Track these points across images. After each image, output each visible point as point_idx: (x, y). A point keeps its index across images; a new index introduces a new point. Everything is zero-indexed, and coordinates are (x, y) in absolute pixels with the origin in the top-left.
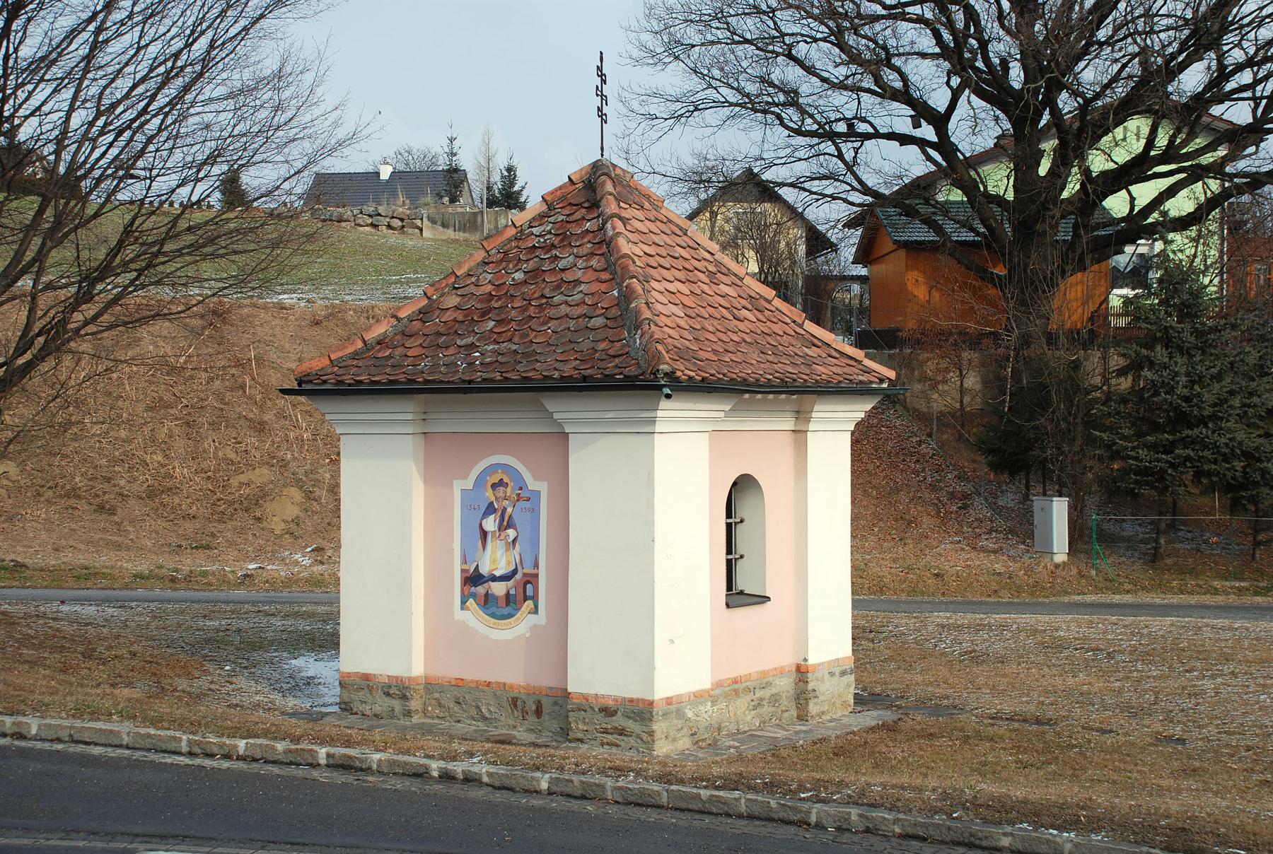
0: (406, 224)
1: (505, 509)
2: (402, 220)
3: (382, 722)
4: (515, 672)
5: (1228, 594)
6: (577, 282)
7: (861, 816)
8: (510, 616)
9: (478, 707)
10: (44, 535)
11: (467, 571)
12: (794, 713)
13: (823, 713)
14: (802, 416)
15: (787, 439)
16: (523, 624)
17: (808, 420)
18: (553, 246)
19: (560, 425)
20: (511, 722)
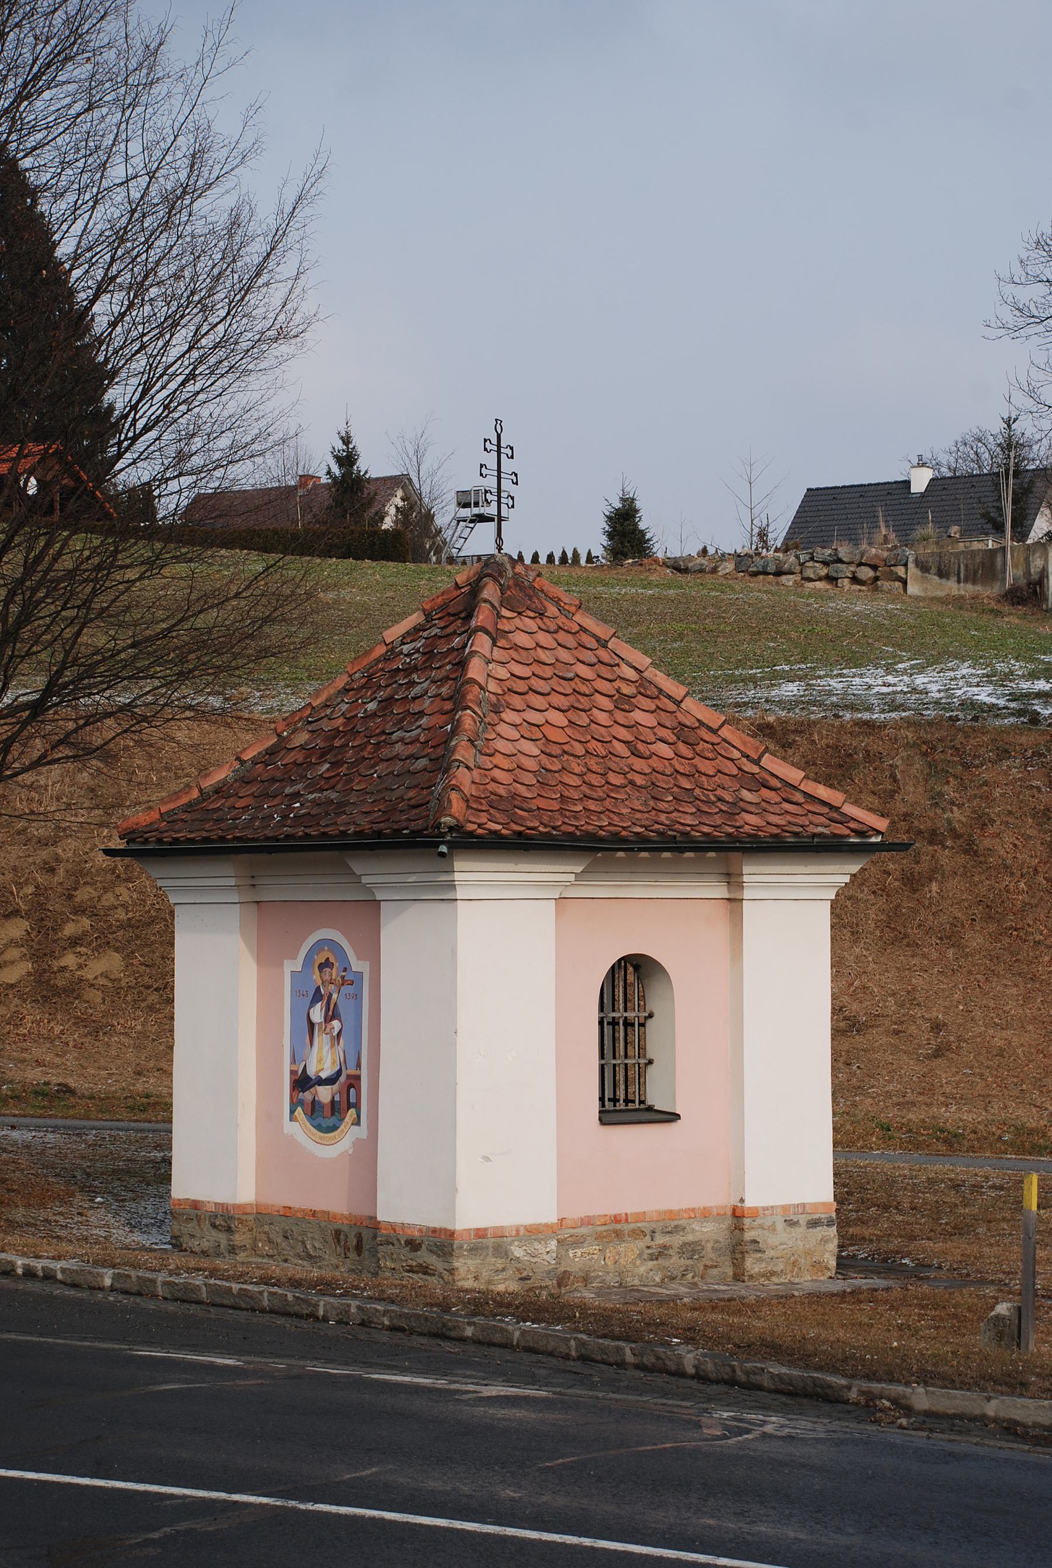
0: (881, 574)
1: (330, 995)
2: (874, 568)
4: (334, 1200)
6: (421, 714)
7: (359, 1307)
8: (334, 1128)
9: (303, 1242)
10: (130, 1055)
12: (730, 1271)
13: (773, 1273)
14: (732, 879)
15: (720, 911)
17: (740, 886)
20: (334, 1261)
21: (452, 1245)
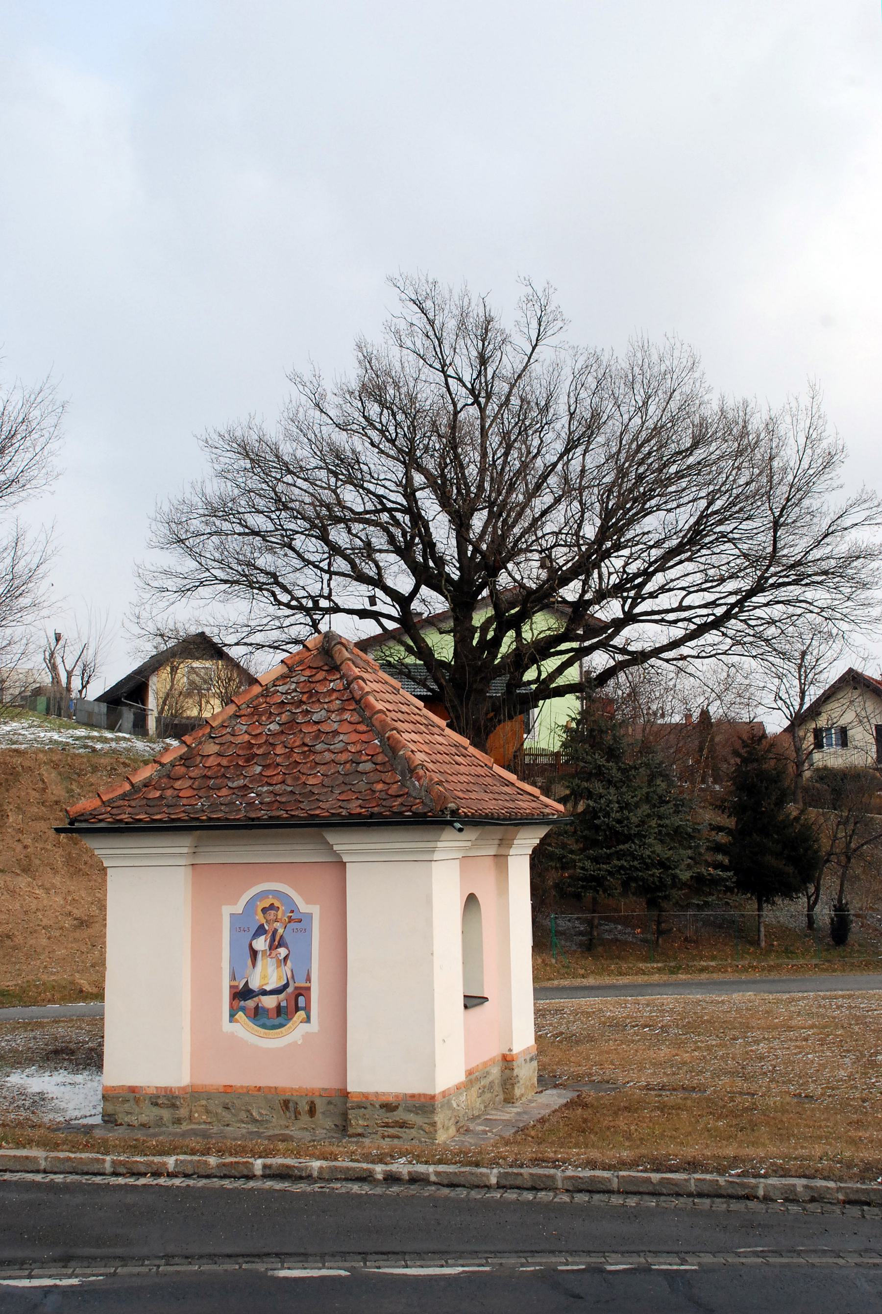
1: (275, 931)
3: (151, 1131)
5: (652, 974)
6: (336, 733)
8: (281, 1026)
11: (237, 987)
15: (489, 862)
16: (297, 1032)
17: (510, 846)
18: (301, 702)
19: (338, 855)
20: (283, 1122)
21: (433, 1106)
